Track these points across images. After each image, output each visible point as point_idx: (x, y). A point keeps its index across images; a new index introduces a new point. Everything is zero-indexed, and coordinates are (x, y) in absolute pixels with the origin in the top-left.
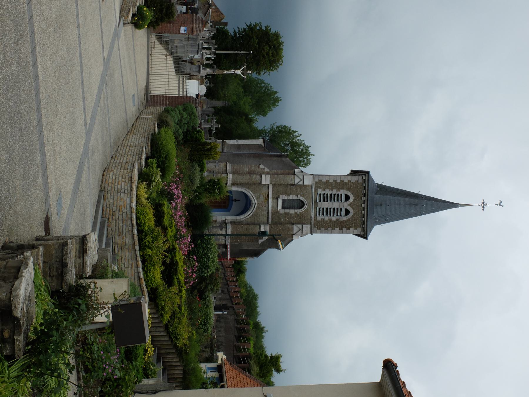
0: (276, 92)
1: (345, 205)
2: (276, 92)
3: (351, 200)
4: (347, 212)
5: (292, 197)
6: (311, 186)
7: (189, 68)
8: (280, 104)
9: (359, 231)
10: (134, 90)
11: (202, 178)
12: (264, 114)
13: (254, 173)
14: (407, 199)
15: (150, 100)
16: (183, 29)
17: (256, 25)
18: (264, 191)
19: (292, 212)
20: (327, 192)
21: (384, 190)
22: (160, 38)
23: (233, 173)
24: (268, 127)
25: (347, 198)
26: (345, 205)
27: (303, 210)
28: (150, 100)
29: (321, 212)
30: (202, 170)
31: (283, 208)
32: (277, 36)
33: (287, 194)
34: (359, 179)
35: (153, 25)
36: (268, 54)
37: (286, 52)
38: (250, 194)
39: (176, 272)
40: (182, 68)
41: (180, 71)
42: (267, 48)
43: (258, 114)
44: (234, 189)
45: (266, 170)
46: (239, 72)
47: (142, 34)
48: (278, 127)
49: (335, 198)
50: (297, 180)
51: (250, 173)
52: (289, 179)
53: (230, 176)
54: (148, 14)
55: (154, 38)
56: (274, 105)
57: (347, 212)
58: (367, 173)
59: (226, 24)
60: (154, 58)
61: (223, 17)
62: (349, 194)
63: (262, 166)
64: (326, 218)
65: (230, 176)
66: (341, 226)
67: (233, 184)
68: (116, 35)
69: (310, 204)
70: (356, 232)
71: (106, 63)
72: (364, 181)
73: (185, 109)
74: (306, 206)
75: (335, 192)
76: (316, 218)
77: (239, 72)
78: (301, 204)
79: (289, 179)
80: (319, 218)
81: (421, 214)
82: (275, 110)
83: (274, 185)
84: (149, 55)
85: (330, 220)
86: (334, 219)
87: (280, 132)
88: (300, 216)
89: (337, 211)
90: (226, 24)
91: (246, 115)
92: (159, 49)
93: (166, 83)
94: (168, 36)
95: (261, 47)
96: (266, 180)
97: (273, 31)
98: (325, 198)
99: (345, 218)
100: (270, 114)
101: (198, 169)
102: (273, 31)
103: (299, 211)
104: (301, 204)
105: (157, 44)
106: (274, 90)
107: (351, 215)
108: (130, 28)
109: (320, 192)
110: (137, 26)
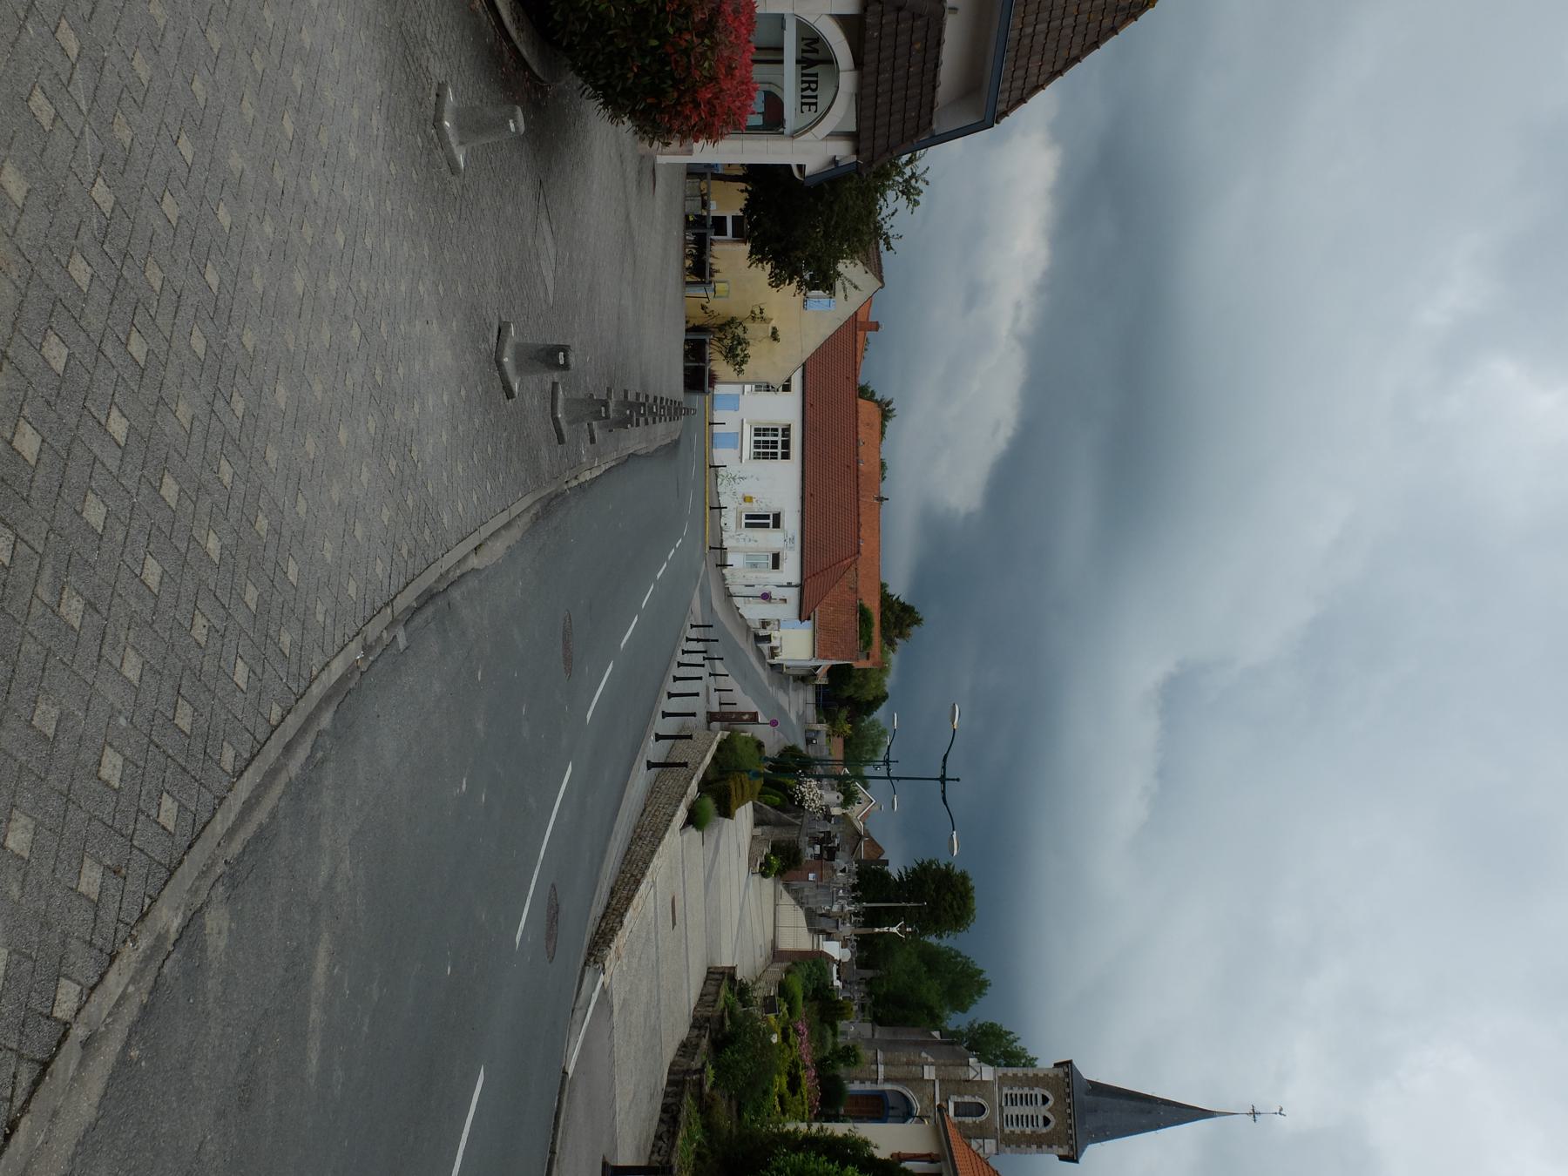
0: (981, 972)
1: (1043, 1111)
2: (981, 972)
3: (1051, 1103)
4: (1046, 1121)
5: (967, 1099)
6: (993, 1083)
7: (825, 924)
8: (989, 991)
9: (1064, 1151)
10: (762, 939)
11: (835, 1044)
12: (964, 1010)
13: (913, 1063)
14: (1133, 1103)
15: (777, 955)
16: (811, 876)
17: (930, 863)
18: (929, 1089)
19: (969, 1120)
20: (1016, 1091)
21: (1098, 1089)
22: (787, 887)
23: (886, 1064)
24: (964, 1027)
25: (1045, 1100)
26: (1043, 1111)
27: (983, 1117)
28: (777, 955)
29: (1010, 1120)
30: (835, 1035)
31: (956, 1115)
32: (964, 877)
33: (960, 1094)
34: (1060, 1072)
35: (780, 873)
36: (951, 906)
37: (979, 902)
38: (909, 1094)
39: (800, 1085)
40: (817, 923)
41: (814, 930)
42: (949, 897)
43: (953, 1010)
44: (888, 1087)
45: (930, 1059)
46: (895, 930)
47: (768, 883)
48: (981, 1026)
49: (1027, 1100)
50: (972, 1074)
51: (908, 1064)
52: (960, 1073)
53: (881, 1068)
54: (775, 861)
55: (781, 887)
56: (980, 993)
57: (1046, 1121)
58: (1070, 1062)
59: (886, 863)
60: (781, 909)
61: (883, 852)
62: (1047, 1094)
63: (924, 1055)
64: (1018, 1130)
65: (881, 1068)
66: (1041, 1142)
67: (886, 1080)
68: (747, 885)
69: (993, 1112)
70: (1062, 1152)
71: (741, 910)
72: (1067, 1075)
73: (815, 964)
74: (988, 1112)
75: (1026, 1091)
76: (1002, 1130)
77: (895, 930)
78: (981, 1110)
79: (960, 1073)
80: (1007, 1131)
81: (1159, 1127)
82: (982, 1001)
83: (942, 1081)
84: (776, 905)
85: (1023, 1133)
86: (1028, 1131)
87: (985, 1034)
88: (981, 1126)
89: (1032, 1120)
90: (886, 863)
91: (930, 1010)
92: (787, 899)
93: (796, 937)
94: (796, 884)
95: (940, 895)
96: (929, 1073)
97: (957, 870)
98: (1013, 1100)
99: (1044, 1130)
100: (973, 1008)
101: (830, 1033)
102: (957, 870)
103: (978, 1120)
104: (981, 1110)
105: (785, 894)
106: (979, 967)
107: (1052, 1125)
108: (757, 877)
109: (1006, 1090)
110: (764, 875)
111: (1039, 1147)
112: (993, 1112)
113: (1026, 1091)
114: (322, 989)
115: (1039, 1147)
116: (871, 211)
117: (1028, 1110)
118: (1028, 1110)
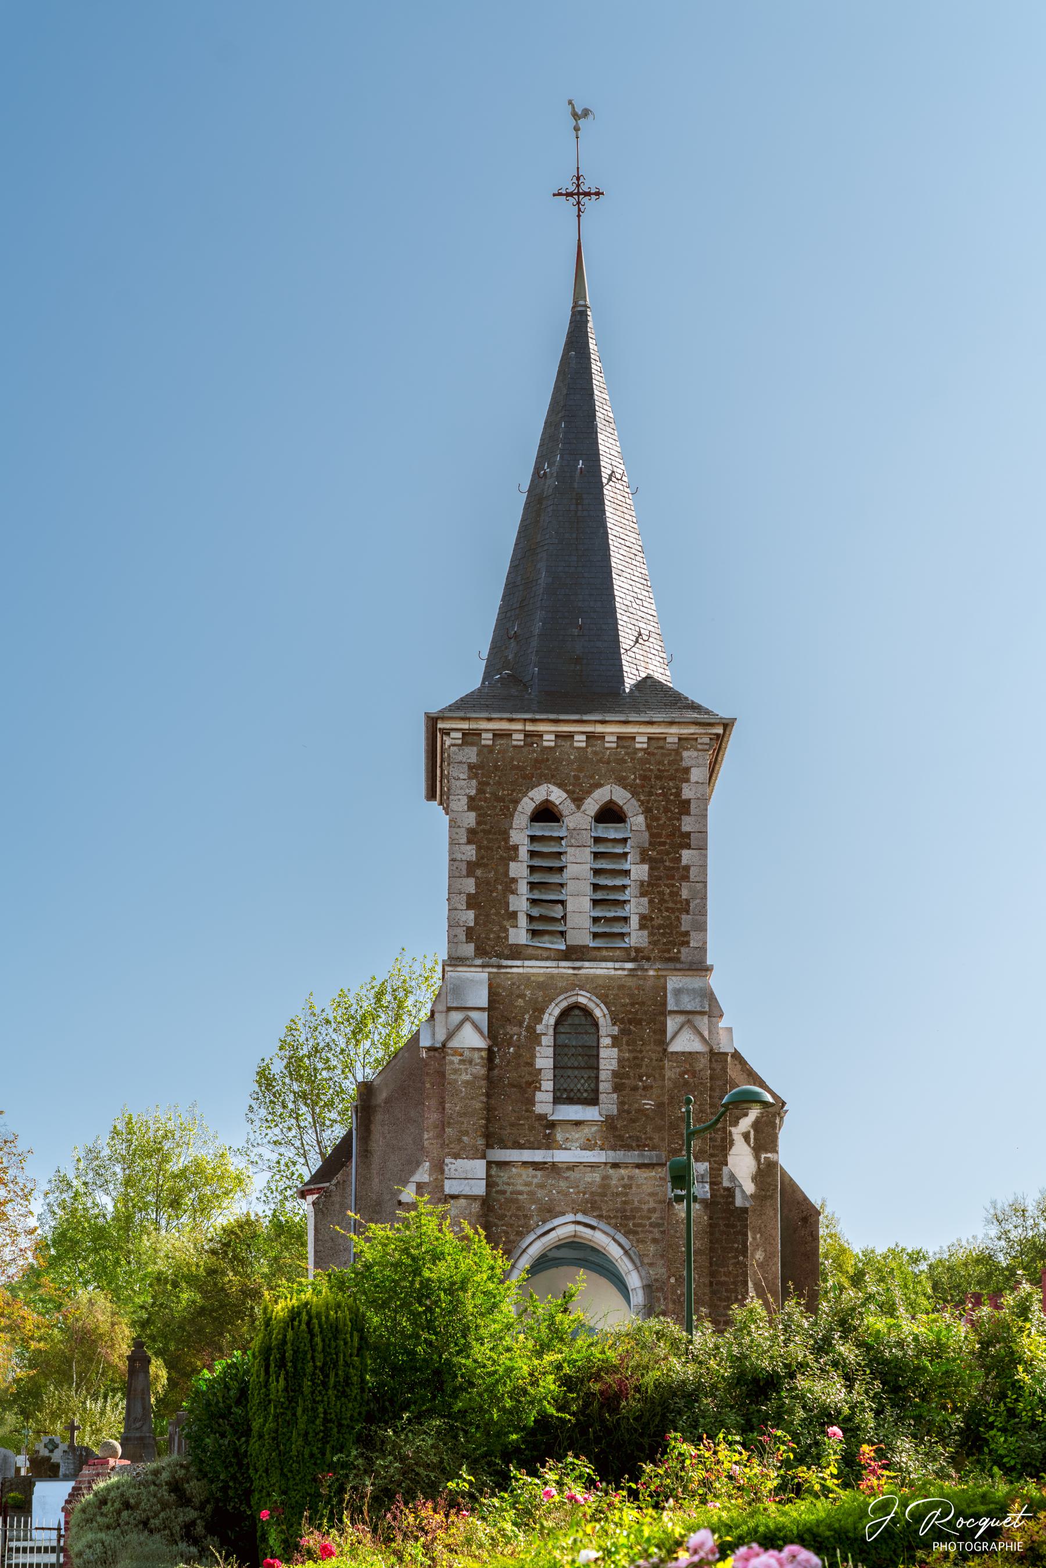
1: (579, 819)
3: (557, 796)
5: (544, 1060)
19: (609, 1058)
20: (520, 903)
25: (546, 813)
27: (600, 1012)
29: (608, 930)
33: (534, 1084)
49: (547, 868)
57: (610, 814)
62: (527, 806)
64: (635, 907)
75: (519, 870)
76: (637, 955)
83: (492, 1139)
86: (640, 872)
98: (546, 922)
99: (637, 821)
103: (607, 1028)
107: (620, 796)
109: (519, 935)
111: (684, 840)
112: (577, 984)
113: (519, 870)
114: (265, 1515)
115: (684, 840)
116: (756, 1185)
117: (579, 866)
118: (579, 866)
